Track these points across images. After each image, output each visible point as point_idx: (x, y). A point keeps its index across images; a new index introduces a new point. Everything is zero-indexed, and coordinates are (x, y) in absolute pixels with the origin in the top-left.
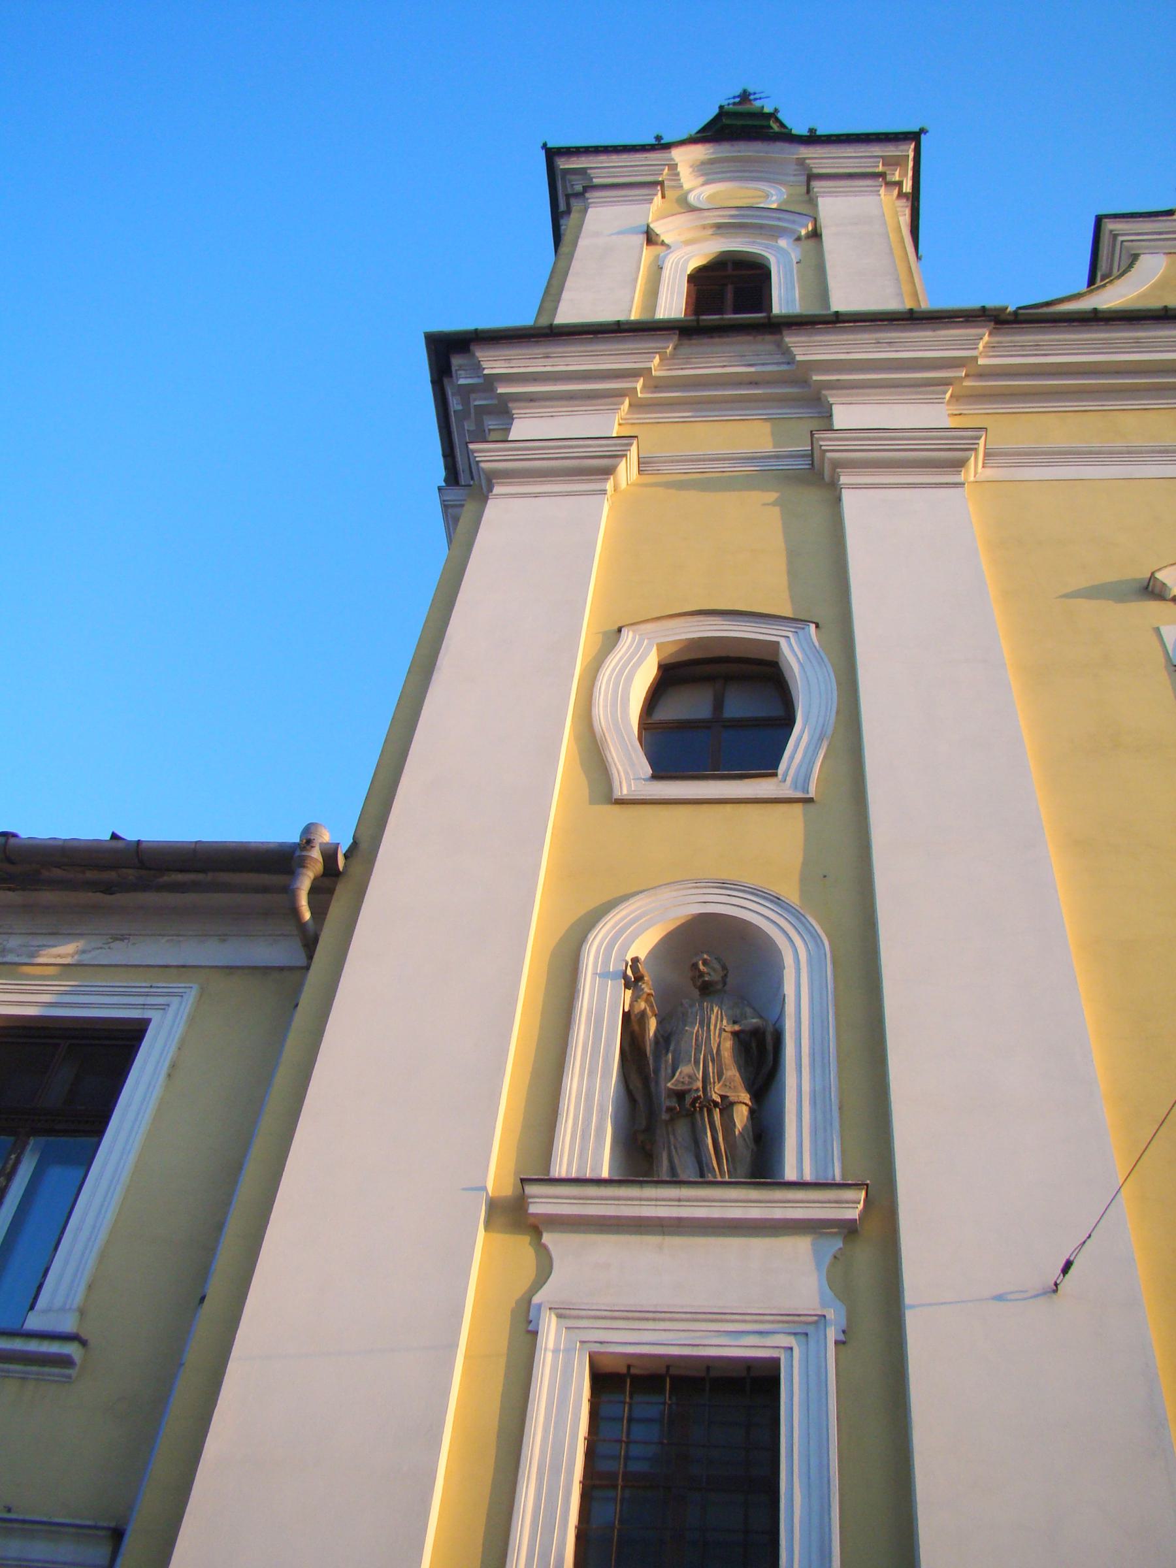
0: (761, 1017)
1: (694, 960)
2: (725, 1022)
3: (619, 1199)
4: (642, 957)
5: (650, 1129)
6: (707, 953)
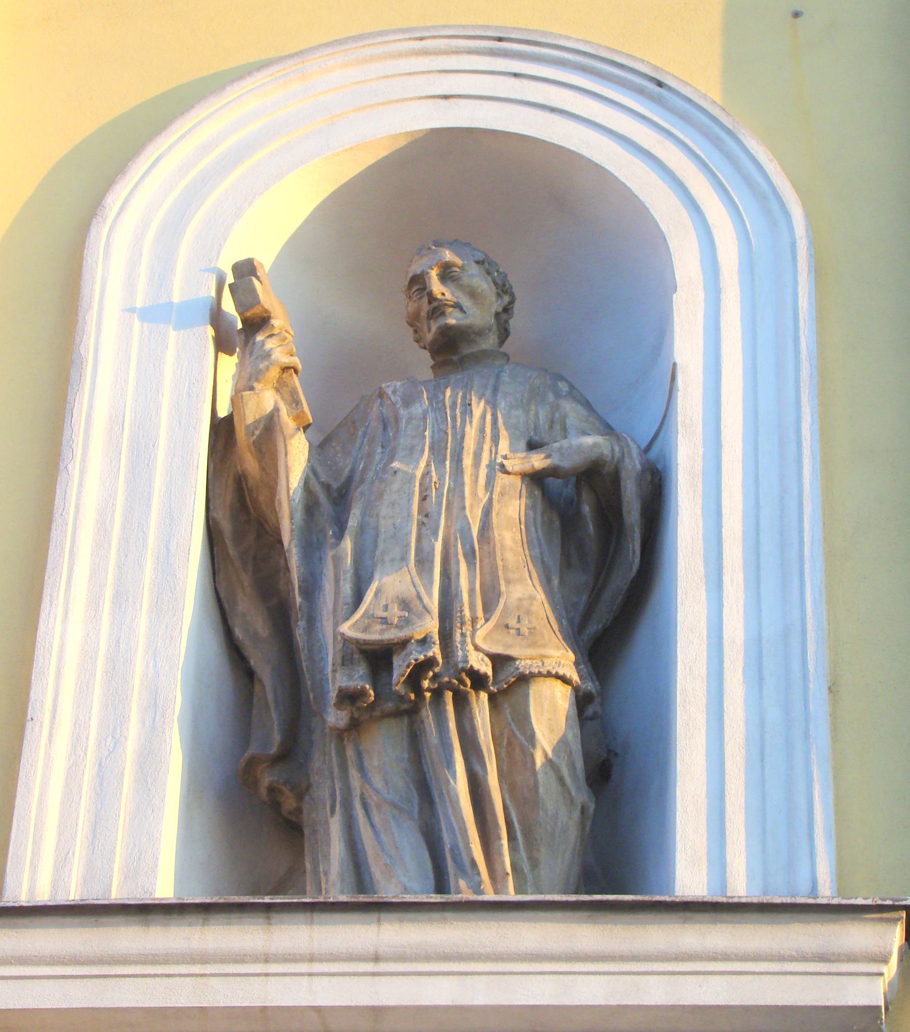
0: (608, 430)
1: (416, 269)
2: (504, 446)
3: (204, 959)
4: (266, 259)
5: (292, 751)
6: (454, 244)
